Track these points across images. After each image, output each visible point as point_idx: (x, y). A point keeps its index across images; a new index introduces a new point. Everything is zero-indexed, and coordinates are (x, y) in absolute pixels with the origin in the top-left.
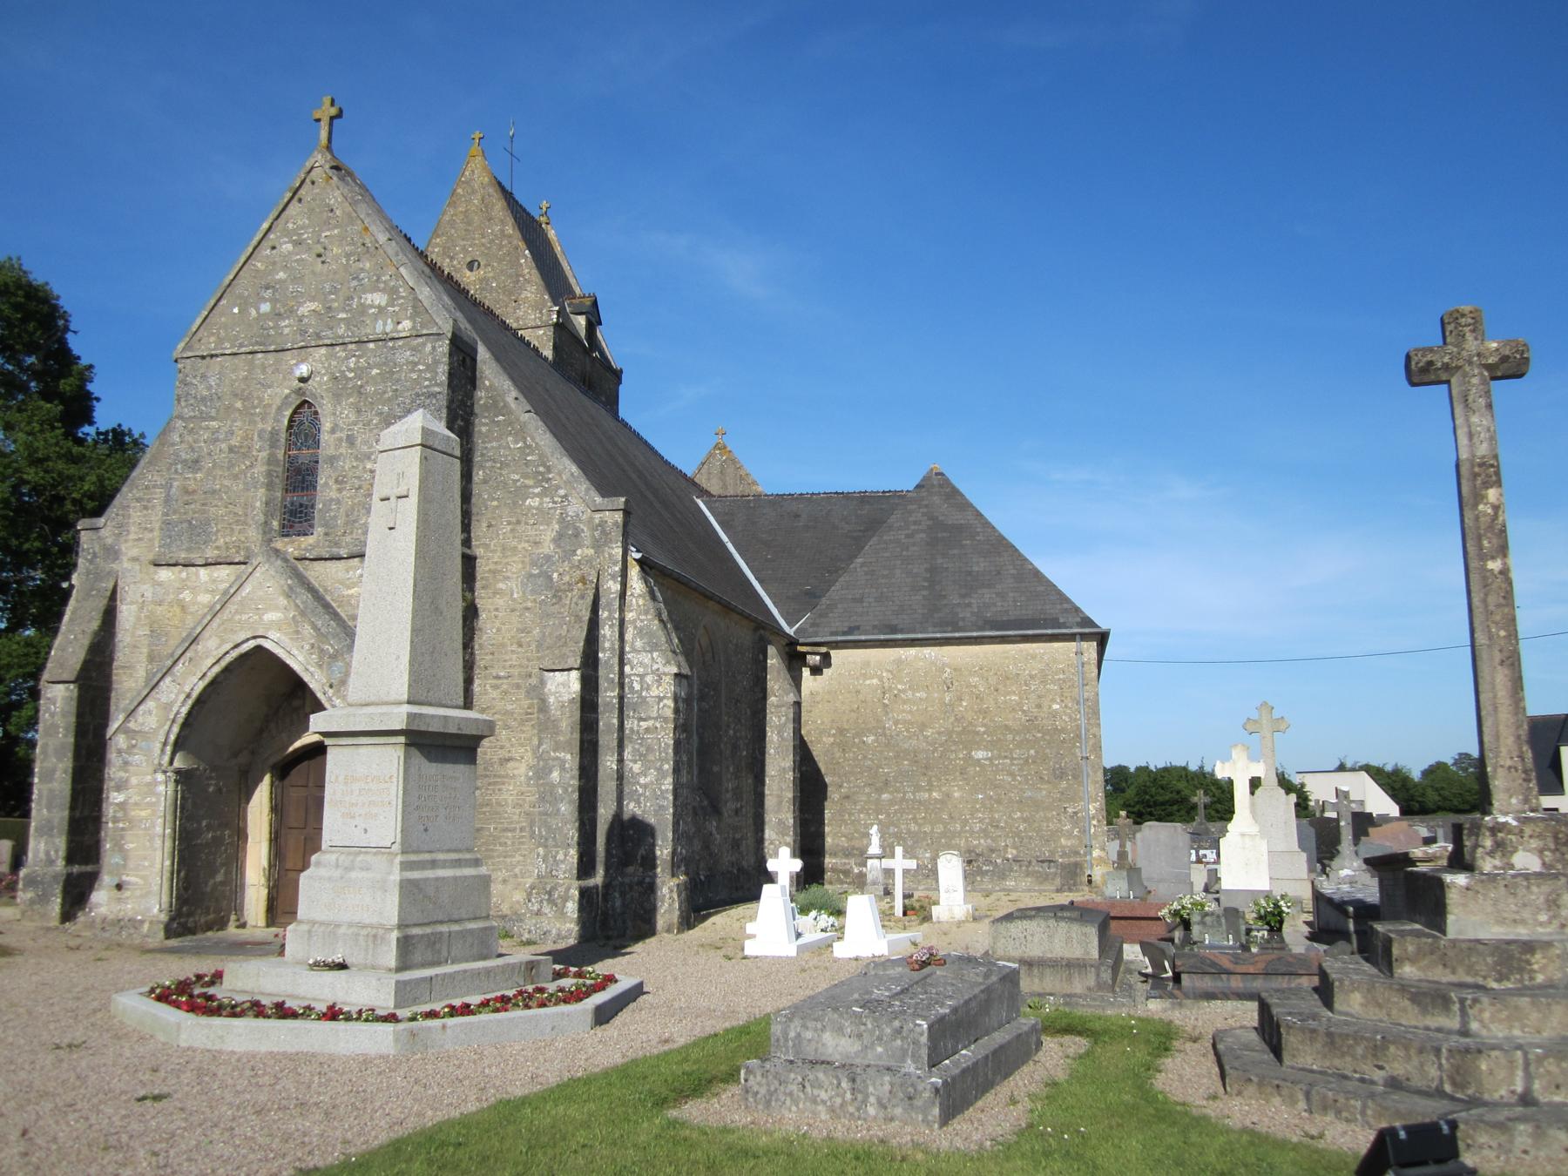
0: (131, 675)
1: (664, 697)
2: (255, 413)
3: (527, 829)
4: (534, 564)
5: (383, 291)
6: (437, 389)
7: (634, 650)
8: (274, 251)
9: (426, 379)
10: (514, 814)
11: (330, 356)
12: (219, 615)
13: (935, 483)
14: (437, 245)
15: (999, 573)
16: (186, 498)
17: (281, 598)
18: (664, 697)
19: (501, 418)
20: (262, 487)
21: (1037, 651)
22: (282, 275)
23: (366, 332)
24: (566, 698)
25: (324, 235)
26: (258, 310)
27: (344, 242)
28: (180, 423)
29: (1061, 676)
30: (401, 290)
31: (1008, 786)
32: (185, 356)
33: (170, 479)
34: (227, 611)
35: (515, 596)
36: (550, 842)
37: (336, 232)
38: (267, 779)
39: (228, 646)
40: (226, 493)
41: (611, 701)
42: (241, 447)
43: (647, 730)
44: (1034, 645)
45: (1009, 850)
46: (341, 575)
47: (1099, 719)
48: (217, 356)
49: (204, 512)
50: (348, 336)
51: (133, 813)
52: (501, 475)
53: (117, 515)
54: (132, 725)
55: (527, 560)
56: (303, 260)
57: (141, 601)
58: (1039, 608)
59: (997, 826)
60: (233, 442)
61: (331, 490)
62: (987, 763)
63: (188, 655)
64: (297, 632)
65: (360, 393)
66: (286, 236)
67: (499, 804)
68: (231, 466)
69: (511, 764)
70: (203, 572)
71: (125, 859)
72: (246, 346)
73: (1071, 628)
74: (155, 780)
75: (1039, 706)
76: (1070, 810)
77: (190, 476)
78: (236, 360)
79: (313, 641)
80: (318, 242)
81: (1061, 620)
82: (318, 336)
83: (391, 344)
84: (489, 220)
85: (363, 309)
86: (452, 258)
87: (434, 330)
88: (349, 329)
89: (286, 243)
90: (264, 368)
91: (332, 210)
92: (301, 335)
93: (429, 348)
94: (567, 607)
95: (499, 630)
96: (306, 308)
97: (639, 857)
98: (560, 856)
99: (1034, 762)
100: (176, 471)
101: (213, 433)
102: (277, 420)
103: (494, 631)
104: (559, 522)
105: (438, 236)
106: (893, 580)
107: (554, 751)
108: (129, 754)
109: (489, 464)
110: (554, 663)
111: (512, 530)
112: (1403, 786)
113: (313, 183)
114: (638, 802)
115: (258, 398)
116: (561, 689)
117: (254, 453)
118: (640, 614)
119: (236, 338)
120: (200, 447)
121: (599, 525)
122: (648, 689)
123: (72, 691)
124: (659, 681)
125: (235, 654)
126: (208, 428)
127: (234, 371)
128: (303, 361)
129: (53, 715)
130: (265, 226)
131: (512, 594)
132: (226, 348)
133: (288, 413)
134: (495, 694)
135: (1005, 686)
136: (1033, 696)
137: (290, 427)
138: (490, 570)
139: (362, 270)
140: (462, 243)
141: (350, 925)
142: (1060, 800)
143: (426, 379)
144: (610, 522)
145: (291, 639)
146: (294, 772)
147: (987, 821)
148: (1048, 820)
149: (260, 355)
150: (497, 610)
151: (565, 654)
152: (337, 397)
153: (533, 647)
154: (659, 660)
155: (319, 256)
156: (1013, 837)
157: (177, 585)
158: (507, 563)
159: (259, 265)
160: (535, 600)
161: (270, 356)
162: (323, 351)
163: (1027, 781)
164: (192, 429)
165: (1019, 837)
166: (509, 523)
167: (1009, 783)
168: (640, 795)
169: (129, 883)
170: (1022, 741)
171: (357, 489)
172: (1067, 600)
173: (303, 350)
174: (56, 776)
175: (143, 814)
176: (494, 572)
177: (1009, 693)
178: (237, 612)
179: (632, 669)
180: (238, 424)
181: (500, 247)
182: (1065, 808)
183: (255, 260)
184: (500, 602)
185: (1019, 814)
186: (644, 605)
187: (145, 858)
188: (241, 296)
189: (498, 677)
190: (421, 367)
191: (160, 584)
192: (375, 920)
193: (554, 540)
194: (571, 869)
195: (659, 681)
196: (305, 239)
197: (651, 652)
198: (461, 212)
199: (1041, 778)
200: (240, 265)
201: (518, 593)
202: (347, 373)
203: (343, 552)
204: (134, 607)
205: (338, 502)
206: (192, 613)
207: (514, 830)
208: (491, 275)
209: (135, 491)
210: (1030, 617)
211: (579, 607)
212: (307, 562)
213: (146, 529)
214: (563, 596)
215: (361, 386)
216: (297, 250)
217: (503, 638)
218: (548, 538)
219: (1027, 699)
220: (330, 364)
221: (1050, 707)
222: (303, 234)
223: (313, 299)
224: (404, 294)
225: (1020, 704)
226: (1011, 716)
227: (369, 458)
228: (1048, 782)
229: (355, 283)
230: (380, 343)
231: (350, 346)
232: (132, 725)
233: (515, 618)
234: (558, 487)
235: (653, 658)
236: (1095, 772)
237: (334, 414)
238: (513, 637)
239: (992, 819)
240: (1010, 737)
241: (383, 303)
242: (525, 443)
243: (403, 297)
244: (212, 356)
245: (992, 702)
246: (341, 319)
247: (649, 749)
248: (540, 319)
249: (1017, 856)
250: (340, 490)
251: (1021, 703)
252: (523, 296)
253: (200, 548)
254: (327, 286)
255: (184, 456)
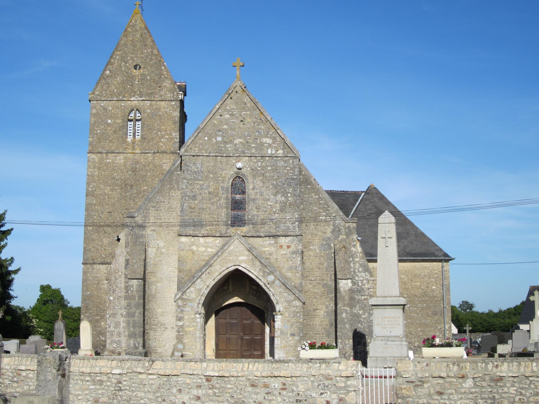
0: (155, 276)
1: (370, 288)
2: (219, 180)
3: (325, 333)
4: (324, 240)
5: (270, 138)
6: (295, 177)
7: (359, 272)
8: (221, 117)
9: (291, 173)
10: (319, 328)
11: (249, 161)
12: (220, 257)
13: (374, 192)
14: (118, 55)
15: (408, 233)
16: (191, 210)
17: (246, 252)
18: (370, 288)
19: (309, 186)
20: (224, 208)
21: (427, 266)
22: (225, 127)
23: (263, 153)
24: (347, 289)
25: (243, 113)
26: (216, 139)
27: (252, 117)
28: (185, 181)
29: (436, 276)
30: (277, 138)
31: (415, 318)
32: (185, 154)
33: (183, 202)
34: (224, 256)
35: (317, 251)
36: (343, 338)
37: (248, 112)
38: (214, 316)
39: (224, 269)
40: (209, 209)
41: (354, 290)
42: (214, 192)
43: (364, 299)
44: (426, 263)
45: (416, 343)
46: (261, 243)
47: (450, 292)
48: (200, 156)
49: (199, 216)
50: (256, 154)
51: (186, 329)
52: (310, 207)
53: (143, 212)
54: (184, 297)
55: (321, 238)
56: (234, 122)
57: (157, 247)
58: (427, 248)
59: (411, 334)
60: (210, 190)
61: (254, 211)
62: (408, 309)
63: (207, 271)
64: (253, 264)
65: (263, 176)
66: (226, 111)
67: (313, 325)
68: (210, 199)
69: (318, 311)
70: (201, 239)
71: (184, 346)
72: (212, 153)
73: (440, 257)
74: (196, 317)
75: (428, 287)
76: (439, 327)
77: (192, 202)
78: (209, 158)
79: (260, 268)
80: (241, 116)
81: (436, 254)
82: (243, 152)
83: (275, 158)
84: (145, 46)
85: (262, 144)
86: (126, 63)
87: (293, 155)
88: (257, 151)
89: (226, 114)
90: (221, 163)
91: (245, 104)
92: (236, 151)
93: (291, 161)
94: (341, 257)
95: (311, 263)
96: (237, 141)
97: (362, 343)
98: (347, 342)
99: (425, 309)
100: (185, 199)
101: (201, 186)
102: (228, 183)
103: (309, 263)
104: (333, 226)
105: (118, 51)
106: (366, 234)
107: (343, 307)
108: (184, 307)
109: (305, 203)
110: (342, 277)
111: (315, 228)
112: (457, 318)
113: (237, 92)
114: (362, 324)
115: (220, 174)
116: (345, 285)
117: (220, 195)
118: (361, 259)
119: (207, 149)
120: (195, 191)
121: (348, 227)
122: (364, 285)
123: (140, 282)
124: (368, 283)
125: (227, 271)
126: (198, 184)
127: (208, 162)
128: (239, 161)
129: (132, 292)
130: (217, 107)
131: (316, 251)
132: (203, 153)
133: (231, 180)
134: (310, 286)
135: (415, 279)
136: (425, 283)
137: (232, 185)
138: (307, 241)
139: (261, 129)
140: (131, 55)
141: (390, 357)
142: (435, 324)
143: (291, 173)
144: (352, 226)
145: (251, 267)
146: (220, 313)
147: (407, 331)
148: (431, 331)
149: (219, 157)
150: (310, 256)
151: (345, 274)
152: (254, 177)
153: (324, 270)
154: (368, 275)
155: (242, 121)
156: (417, 338)
157: (190, 243)
158: (314, 239)
159: (215, 121)
160: (325, 253)
161: (223, 158)
162: (247, 158)
163: (423, 316)
164: (191, 184)
165: (420, 338)
166: (314, 225)
167: (416, 317)
168: (363, 322)
169: (186, 355)
170: (421, 301)
171: (265, 212)
172: (437, 246)
173: (238, 157)
174: (136, 315)
175: (191, 329)
176: (309, 242)
177: (416, 282)
178: (227, 256)
179: (358, 278)
180: (212, 183)
181: (152, 60)
182: (437, 327)
183: (213, 119)
184: (311, 253)
185: (420, 329)
186: (362, 256)
187: (193, 346)
188: (208, 133)
189: (311, 280)
190: (288, 168)
191: (182, 243)
192: (399, 355)
193: (331, 232)
194: (351, 346)
195: (368, 283)
196: (235, 114)
197: (365, 272)
198: (130, 40)
199: (428, 315)
200: (207, 121)
201: (318, 250)
202: (258, 168)
203: (262, 235)
204: (154, 249)
205: (257, 216)
206: (197, 254)
207: (320, 334)
208: (147, 73)
209: (152, 203)
210: (424, 252)
211: (346, 257)
212: (247, 237)
213: (158, 218)
214: (339, 253)
215: (264, 173)
216: (231, 117)
217: (313, 266)
218: (329, 231)
219: (423, 284)
220: (250, 164)
221: (432, 287)
222: (234, 112)
223: (240, 138)
224: (279, 140)
225: (420, 286)
226: (417, 290)
227: (269, 200)
228: (431, 317)
229: (257, 133)
230: (271, 158)
231: (258, 158)
232: (184, 297)
233: (317, 260)
234: (332, 213)
235: (366, 275)
236: (448, 313)
237: (253, 183)
238: (316, 266)
239: (409, 331)
240: (416, 299)
241: (271, 143)
242: (319, 196)
243: (279, 141)
244: (198, 156)
245: (410, 285)
246: (253, 147)
247: (365, 306)
248: (173, 97)
249: (419, 345)
250: (258, 212)
251: (421, 286)
252: (164, 85)
253: (199, 230)
254: (246, 133)
255: (188, 194)
